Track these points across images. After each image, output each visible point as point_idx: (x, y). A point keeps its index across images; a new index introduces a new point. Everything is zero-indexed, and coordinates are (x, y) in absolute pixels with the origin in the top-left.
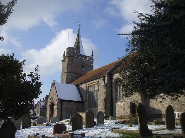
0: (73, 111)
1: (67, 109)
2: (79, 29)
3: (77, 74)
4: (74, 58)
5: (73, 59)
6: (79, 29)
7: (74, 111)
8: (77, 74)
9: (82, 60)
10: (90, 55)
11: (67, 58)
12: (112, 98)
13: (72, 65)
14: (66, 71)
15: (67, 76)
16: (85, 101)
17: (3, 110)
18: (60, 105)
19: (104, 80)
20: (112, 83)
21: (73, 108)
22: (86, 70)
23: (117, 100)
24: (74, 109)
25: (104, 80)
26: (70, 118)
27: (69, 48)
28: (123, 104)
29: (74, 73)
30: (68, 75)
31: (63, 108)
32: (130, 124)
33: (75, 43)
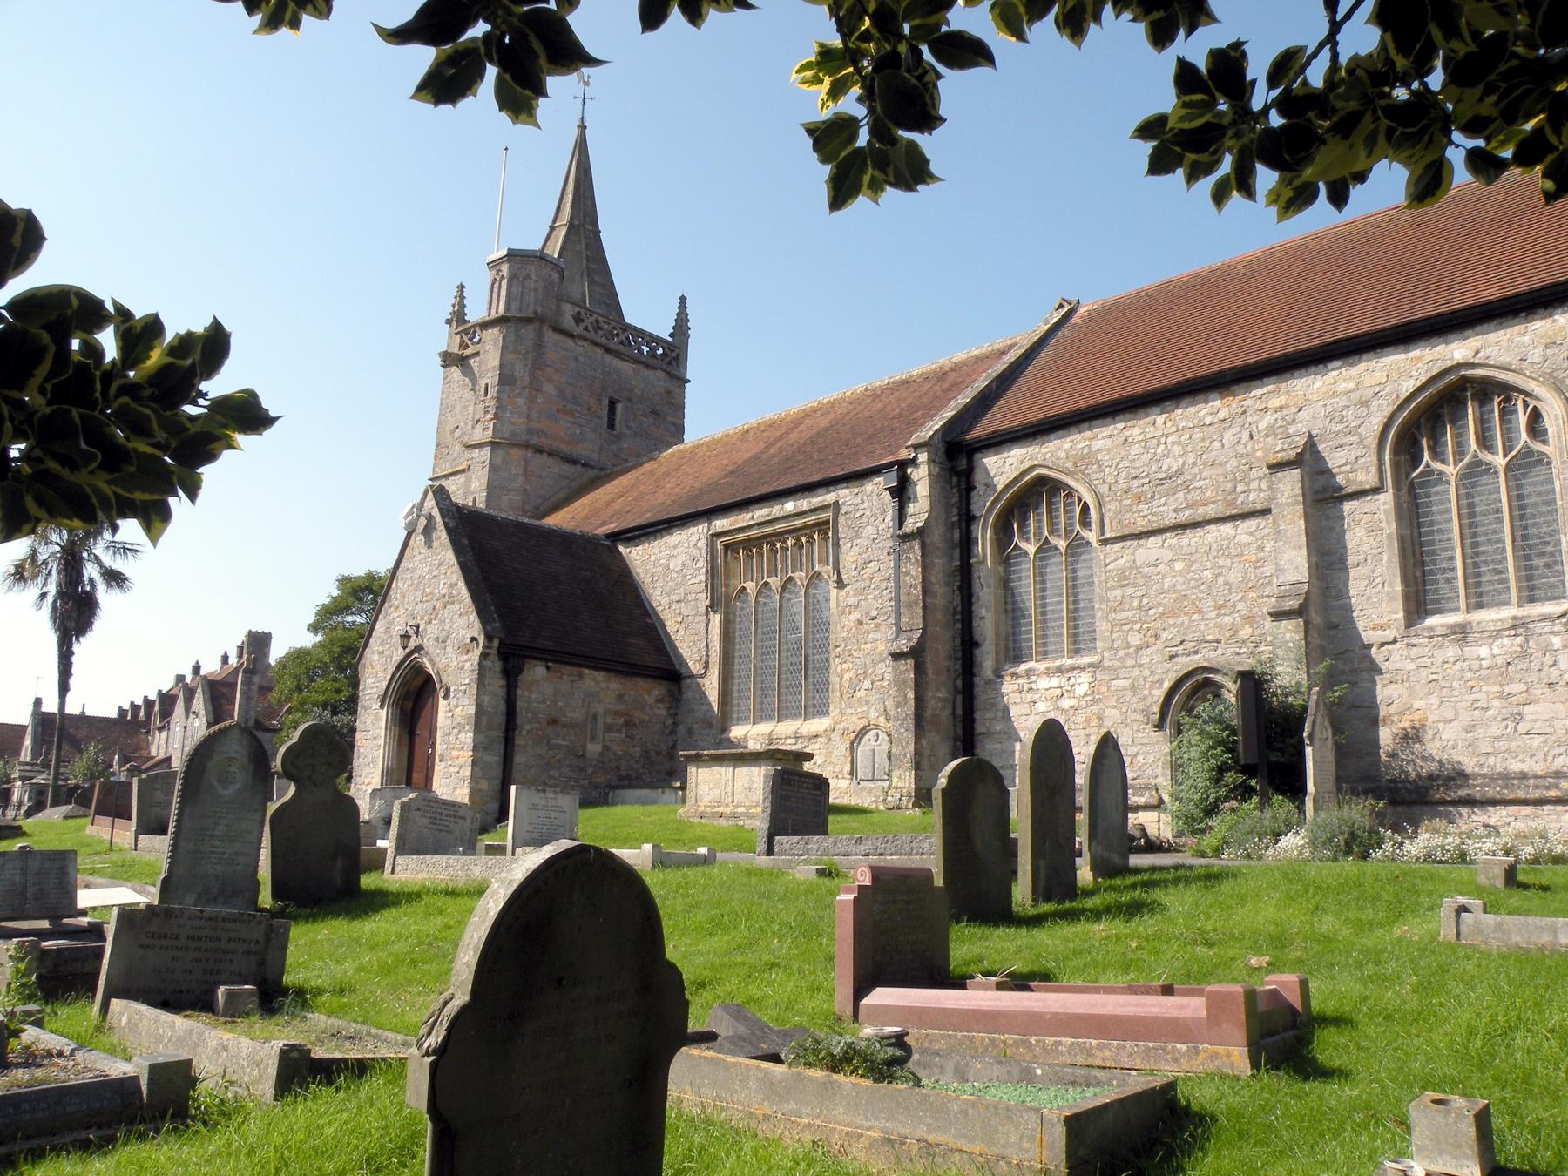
0: (593, 738)
1: (553, 722)
2: (583, 128)
3: (571, 461)
4: (550, 337)
5: (539, 345)
6: (583, 128)
7: (606, 748)
8: (571, 461)
9: (608, 357)
10: (662, 328)
11: (492, 341)
12: (968, 645)
13: (535, 387)
14: (483, 434)
15: (493, 468)
16: (695, 668)
17: (1276, 120)
18: (497, 684)
19: (901, 492)
20: (968, 519)
21: (595, 718)
22: (636, 435)
23: (1012, 653)
24: (609, 728)
25: (901, 492)
26: (70, 411)
27: (513, 256)
28: (1081, 689)
29: (550, 454)
30: (498, 461)
31: (522, 716)
32: (482, 640)
33: (552, 228)
